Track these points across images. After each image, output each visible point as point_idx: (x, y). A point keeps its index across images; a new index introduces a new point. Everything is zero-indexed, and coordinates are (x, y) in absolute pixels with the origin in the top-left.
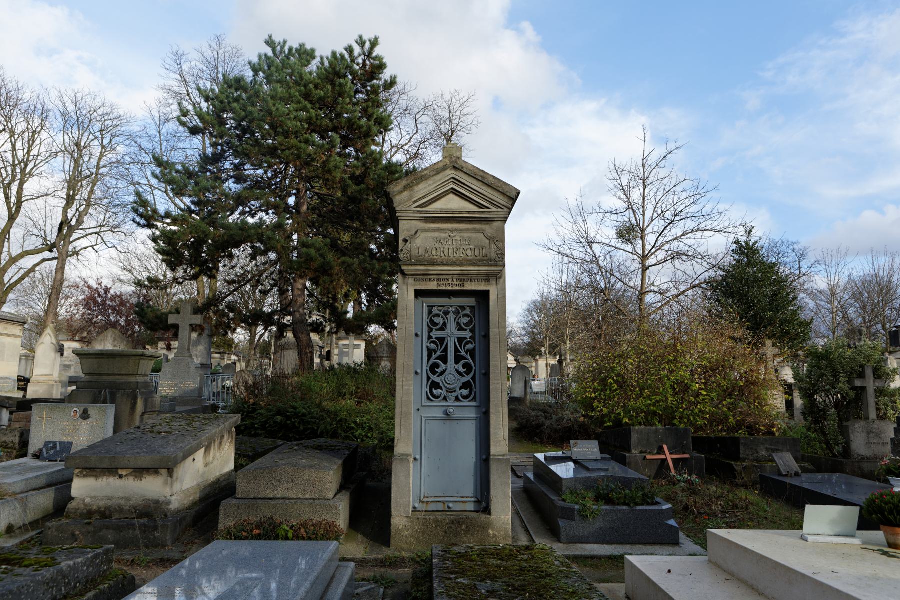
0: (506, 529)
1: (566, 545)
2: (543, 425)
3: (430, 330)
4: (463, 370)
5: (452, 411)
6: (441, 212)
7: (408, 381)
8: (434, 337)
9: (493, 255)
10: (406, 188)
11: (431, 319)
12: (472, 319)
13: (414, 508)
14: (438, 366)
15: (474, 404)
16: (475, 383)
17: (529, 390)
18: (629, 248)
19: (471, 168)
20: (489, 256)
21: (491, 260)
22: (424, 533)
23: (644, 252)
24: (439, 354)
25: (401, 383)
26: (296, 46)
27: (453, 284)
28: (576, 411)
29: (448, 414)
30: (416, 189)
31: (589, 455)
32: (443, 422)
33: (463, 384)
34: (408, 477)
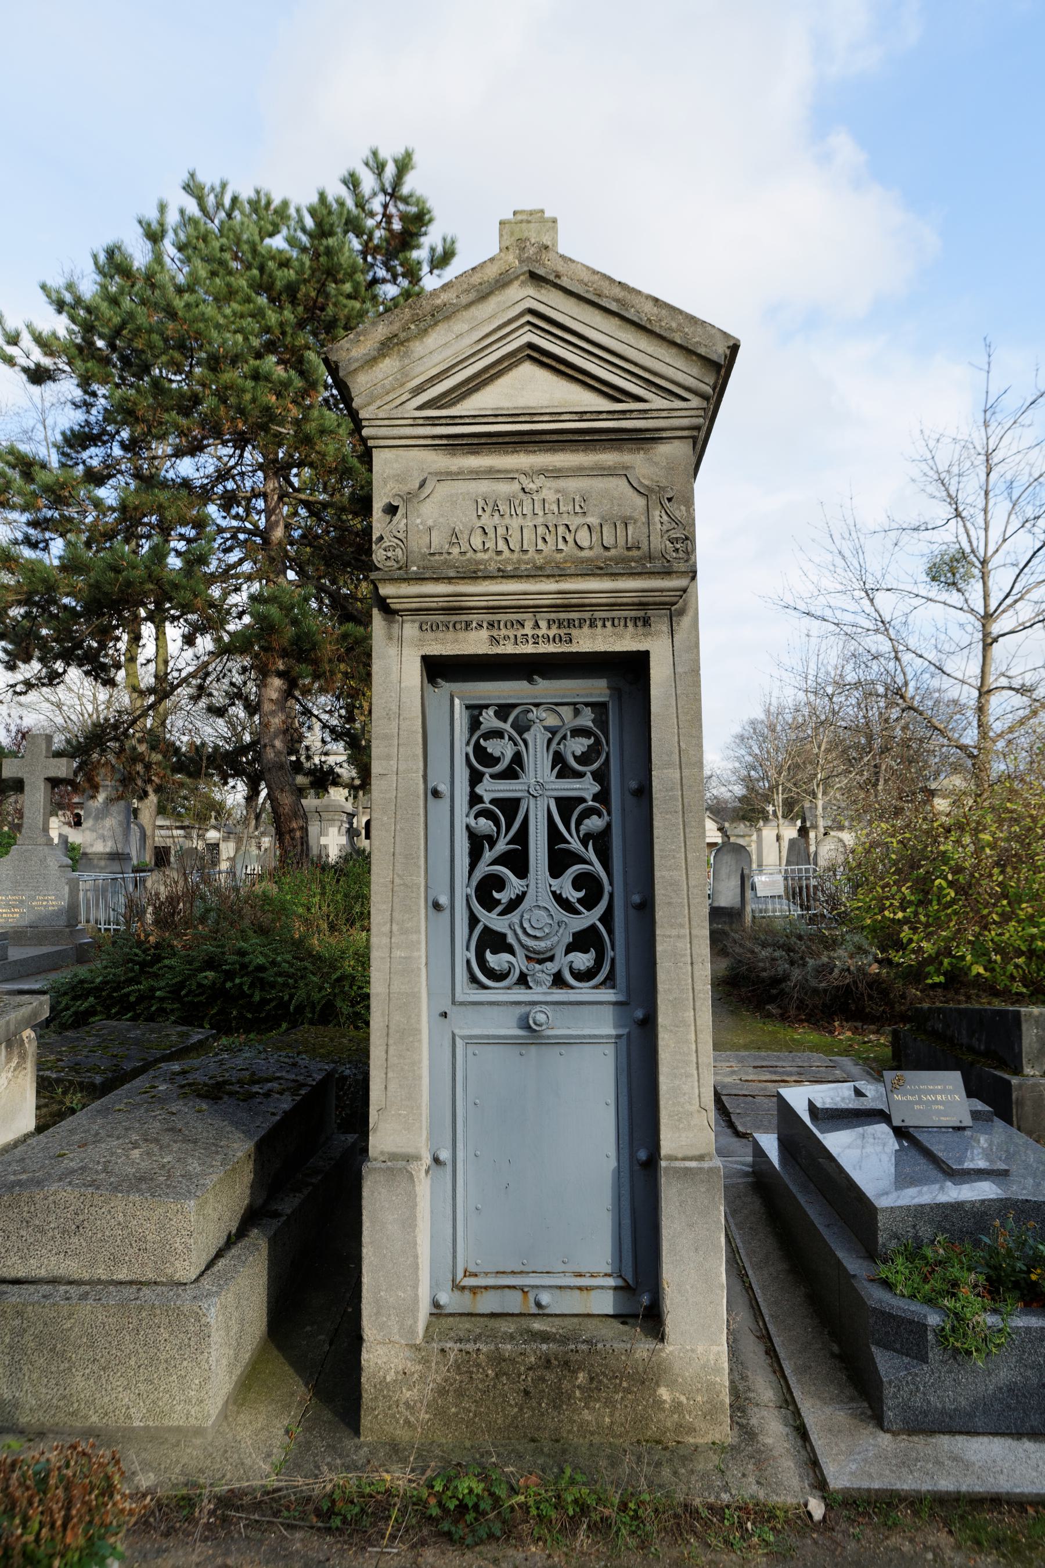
0: (710, 1386)
1: (904, 1442)
2: (786, 977)
3: (475, 778)
4: (573, 895)
5: (541, 1018)
6: (496, 416)
7: (405, 932)
8: (487, 798)
9: (658, 543)
10: (387, 346)
11: (477, 742)
12: (598, 741)
13: (436, 1304)
14: (499, 883)
15: (608, 995)
16: (610, 932)
17: (749, 894)
18: (955, 598)
19: (586, 276)
20: (644, 546)
21: (650, 558)
22: (460, 1393)
23: (986, 606)
24: (501, 846)
25: (385, 940)
26: (246, 193)
27: (535, 637)
28: (860, 949)
29: (529, 1028)
30: (418, 348)
31: (939, 1113)
32: (516, 1050)
33: (575, 935)
34: (409, 1223)
